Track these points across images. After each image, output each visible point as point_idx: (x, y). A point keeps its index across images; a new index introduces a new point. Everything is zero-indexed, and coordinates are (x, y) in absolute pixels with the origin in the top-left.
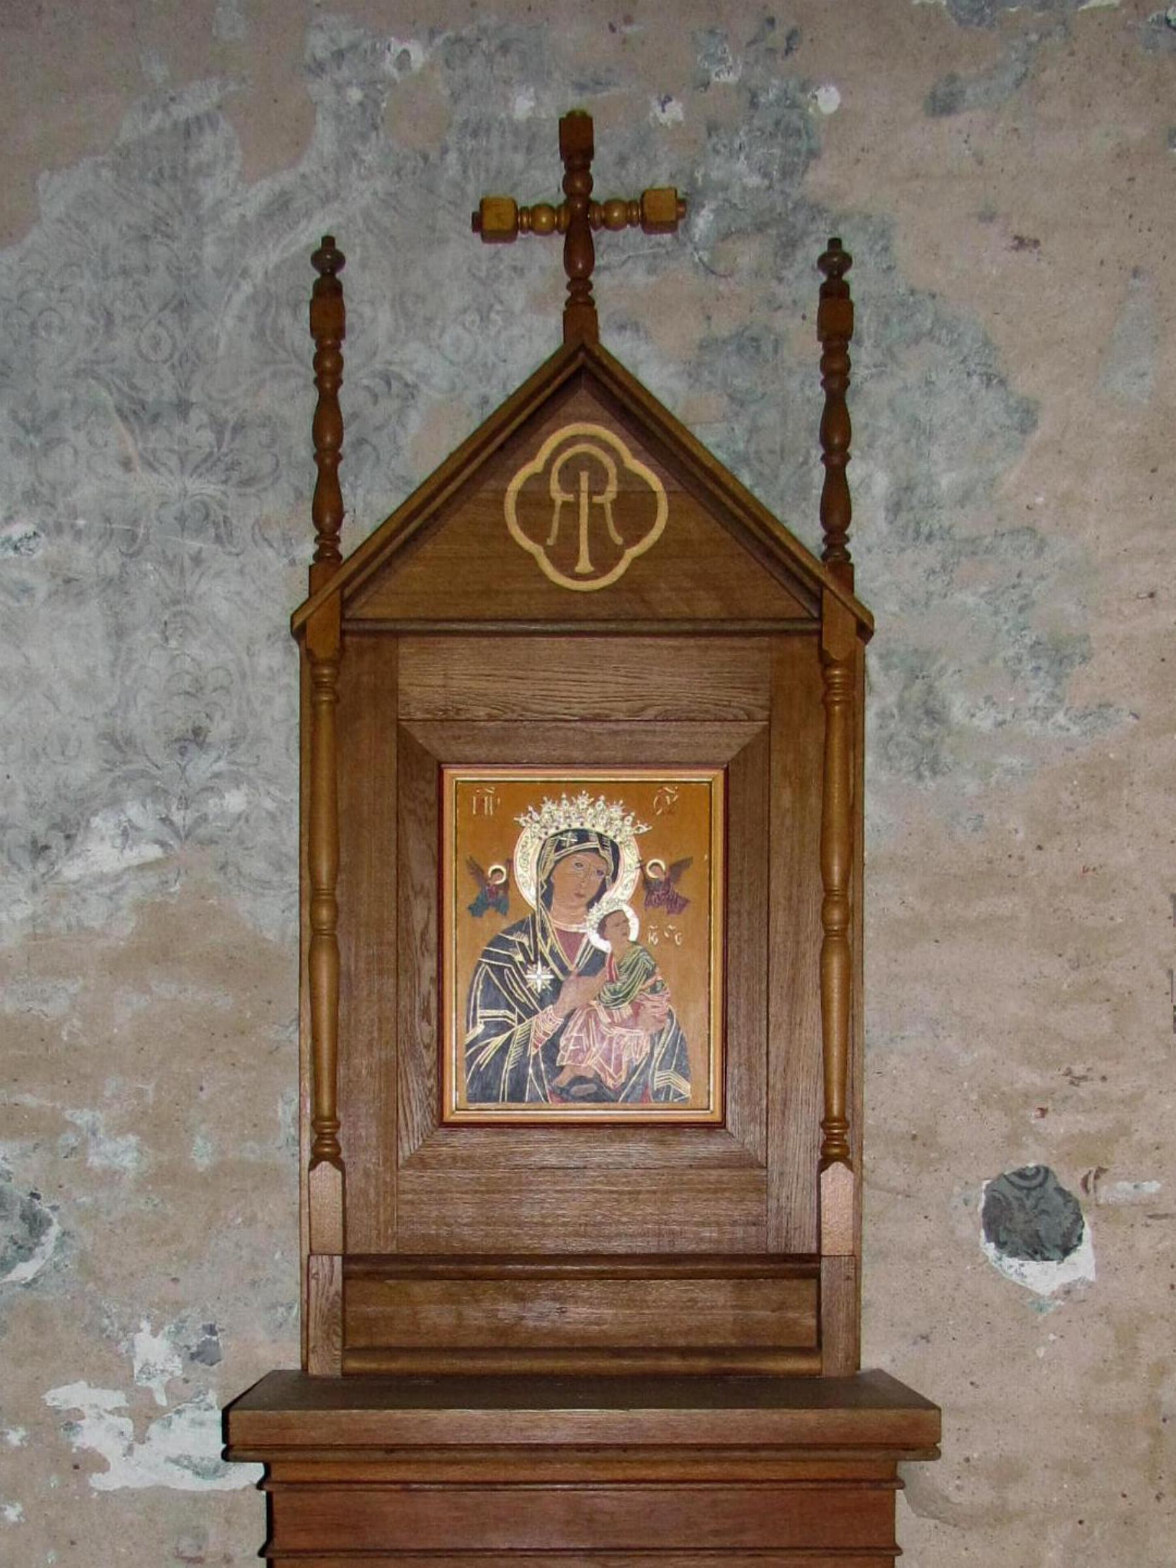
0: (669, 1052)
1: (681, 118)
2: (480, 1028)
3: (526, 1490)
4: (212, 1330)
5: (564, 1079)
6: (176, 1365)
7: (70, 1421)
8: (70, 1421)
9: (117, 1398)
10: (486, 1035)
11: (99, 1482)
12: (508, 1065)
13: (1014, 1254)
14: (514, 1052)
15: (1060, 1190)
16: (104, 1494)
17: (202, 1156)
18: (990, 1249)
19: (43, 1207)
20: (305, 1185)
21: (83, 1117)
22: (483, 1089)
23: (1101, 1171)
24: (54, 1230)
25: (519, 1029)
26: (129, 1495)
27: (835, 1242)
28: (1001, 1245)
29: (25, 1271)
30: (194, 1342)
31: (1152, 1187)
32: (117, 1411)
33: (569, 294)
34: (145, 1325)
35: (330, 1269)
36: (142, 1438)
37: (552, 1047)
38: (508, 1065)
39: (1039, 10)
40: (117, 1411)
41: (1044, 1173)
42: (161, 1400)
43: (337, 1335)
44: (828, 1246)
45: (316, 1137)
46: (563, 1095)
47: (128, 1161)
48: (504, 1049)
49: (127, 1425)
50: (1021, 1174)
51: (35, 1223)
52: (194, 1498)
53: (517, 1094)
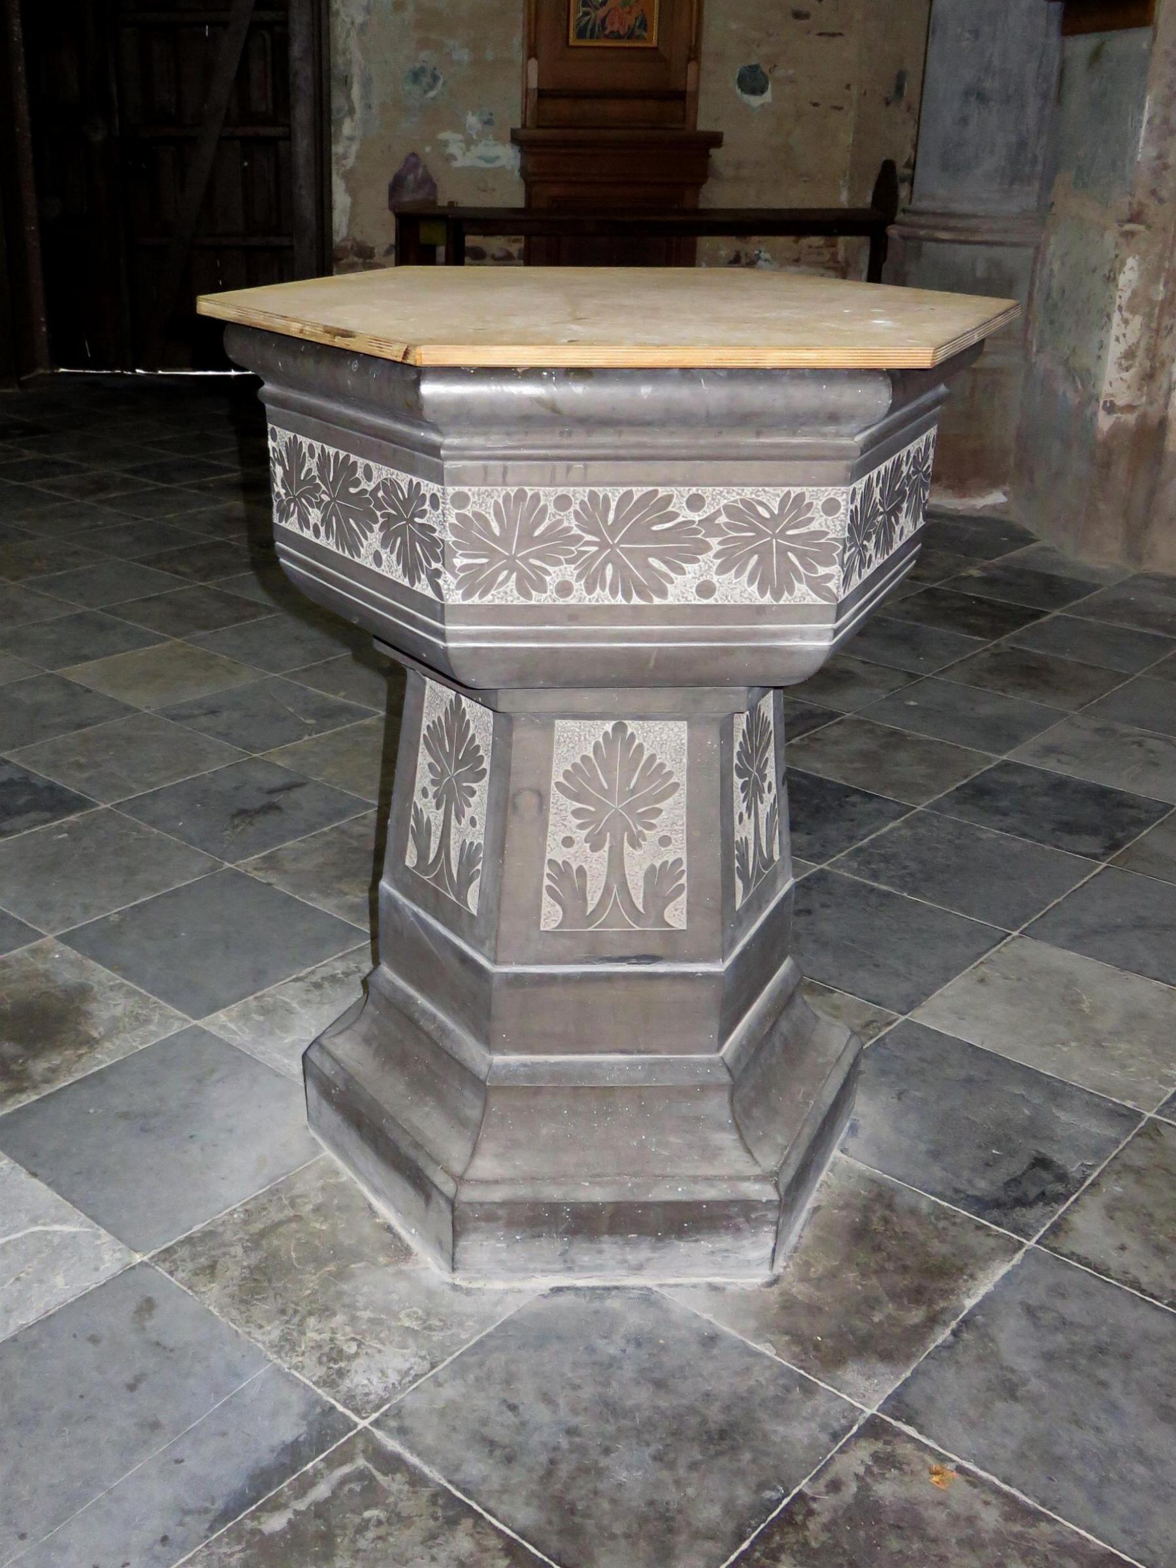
0: (641, 24)
1: (456, 164)
2: (581, 14)
3: (688, 373)
4: (491, 114)
5: (607, 32)
6: (479, 126)
7: (445, 144)
8: (445, 144)
9: (460, 137)
10: (583, 16)
11: (456, 164)
12: (590, 27)
13: (746, 93)
14: (591, 23)
15: (762, 73)
16: (456, 168)
17: (489, 55)
18: (739, 91)
19: (437, 72)
20: (525, 68)
21: (451, 43)
22: (581, 34)
23: (775, 66)
24: (441, 81)
25: (593, 15)
26: (463, 168)
27: (690, 88)
28: (742, 90)
29: (432, 94)
30: (485, 118)
31: (791, 72)
32: (461, 141)
33: (446, 205)
34: (470, 113)
35: (533, 98)
36: (468, 149)
37: (603, 21)
38: (590, 27)
39: (357, 256)
40: (461, 141)
41: (757, 67)
42: (475, 137)
43: (721, 1127)
44: (689, 89)
45: (889, 381)
46: (607, 37)
47: (466, 57)
48: (589, 21)
49: (463, 145)
50: (750, 67)
51: (435, 78)
52: (483, 170)
53: (592, 37)
